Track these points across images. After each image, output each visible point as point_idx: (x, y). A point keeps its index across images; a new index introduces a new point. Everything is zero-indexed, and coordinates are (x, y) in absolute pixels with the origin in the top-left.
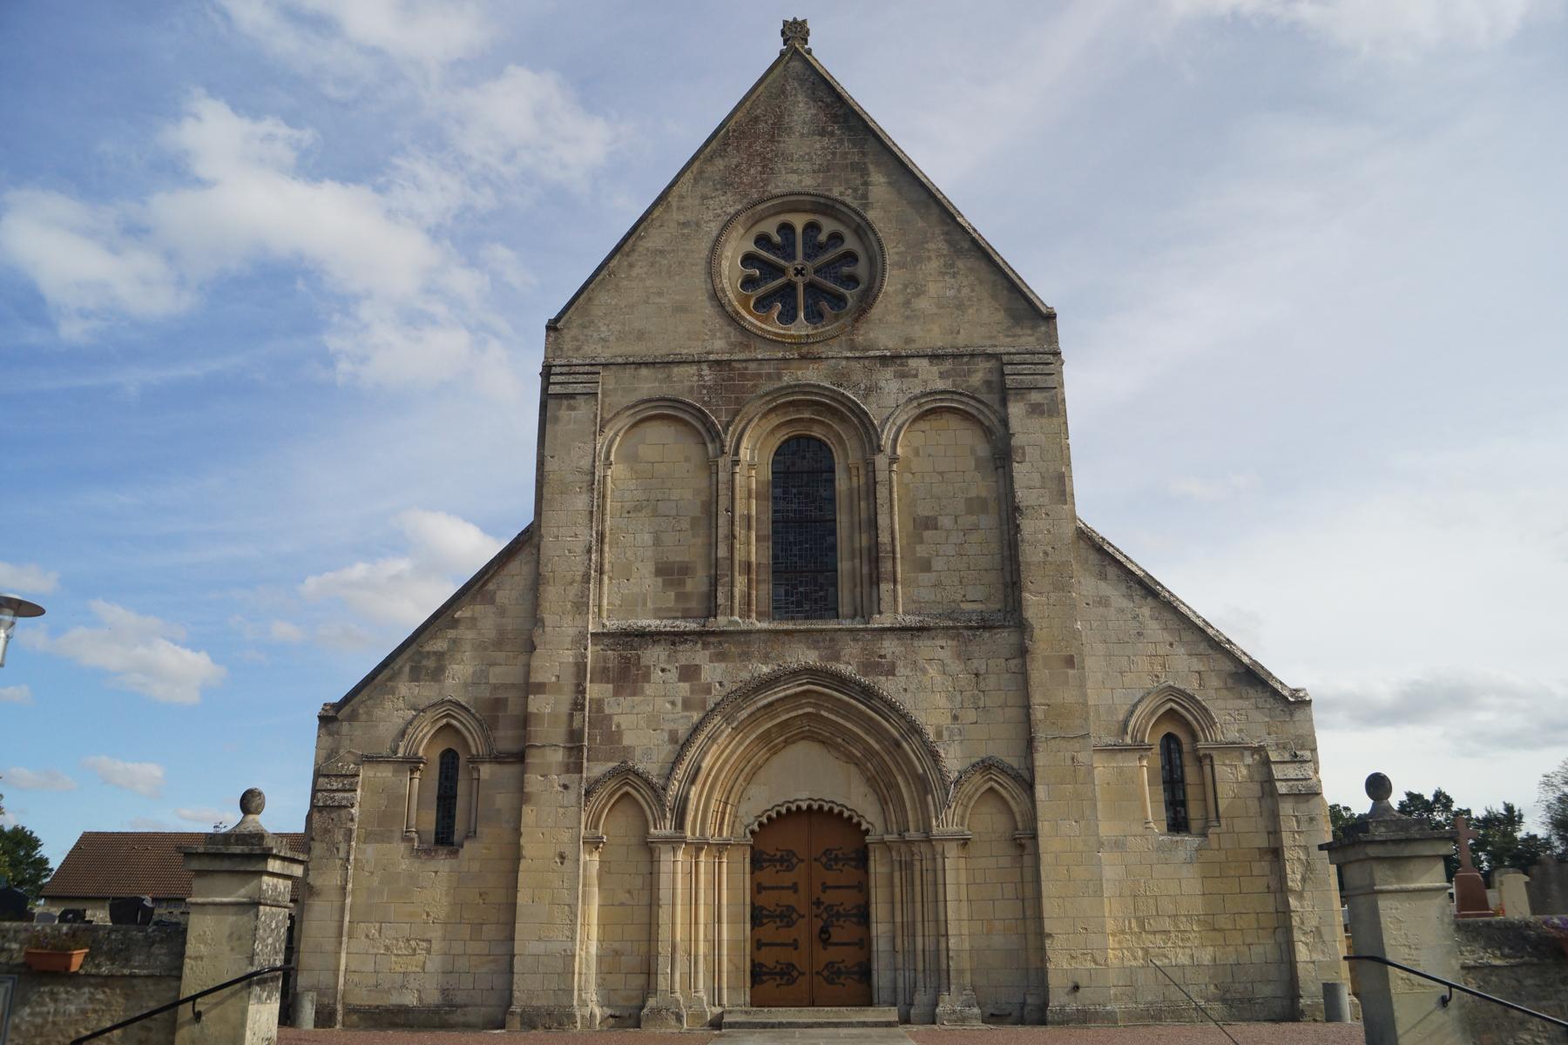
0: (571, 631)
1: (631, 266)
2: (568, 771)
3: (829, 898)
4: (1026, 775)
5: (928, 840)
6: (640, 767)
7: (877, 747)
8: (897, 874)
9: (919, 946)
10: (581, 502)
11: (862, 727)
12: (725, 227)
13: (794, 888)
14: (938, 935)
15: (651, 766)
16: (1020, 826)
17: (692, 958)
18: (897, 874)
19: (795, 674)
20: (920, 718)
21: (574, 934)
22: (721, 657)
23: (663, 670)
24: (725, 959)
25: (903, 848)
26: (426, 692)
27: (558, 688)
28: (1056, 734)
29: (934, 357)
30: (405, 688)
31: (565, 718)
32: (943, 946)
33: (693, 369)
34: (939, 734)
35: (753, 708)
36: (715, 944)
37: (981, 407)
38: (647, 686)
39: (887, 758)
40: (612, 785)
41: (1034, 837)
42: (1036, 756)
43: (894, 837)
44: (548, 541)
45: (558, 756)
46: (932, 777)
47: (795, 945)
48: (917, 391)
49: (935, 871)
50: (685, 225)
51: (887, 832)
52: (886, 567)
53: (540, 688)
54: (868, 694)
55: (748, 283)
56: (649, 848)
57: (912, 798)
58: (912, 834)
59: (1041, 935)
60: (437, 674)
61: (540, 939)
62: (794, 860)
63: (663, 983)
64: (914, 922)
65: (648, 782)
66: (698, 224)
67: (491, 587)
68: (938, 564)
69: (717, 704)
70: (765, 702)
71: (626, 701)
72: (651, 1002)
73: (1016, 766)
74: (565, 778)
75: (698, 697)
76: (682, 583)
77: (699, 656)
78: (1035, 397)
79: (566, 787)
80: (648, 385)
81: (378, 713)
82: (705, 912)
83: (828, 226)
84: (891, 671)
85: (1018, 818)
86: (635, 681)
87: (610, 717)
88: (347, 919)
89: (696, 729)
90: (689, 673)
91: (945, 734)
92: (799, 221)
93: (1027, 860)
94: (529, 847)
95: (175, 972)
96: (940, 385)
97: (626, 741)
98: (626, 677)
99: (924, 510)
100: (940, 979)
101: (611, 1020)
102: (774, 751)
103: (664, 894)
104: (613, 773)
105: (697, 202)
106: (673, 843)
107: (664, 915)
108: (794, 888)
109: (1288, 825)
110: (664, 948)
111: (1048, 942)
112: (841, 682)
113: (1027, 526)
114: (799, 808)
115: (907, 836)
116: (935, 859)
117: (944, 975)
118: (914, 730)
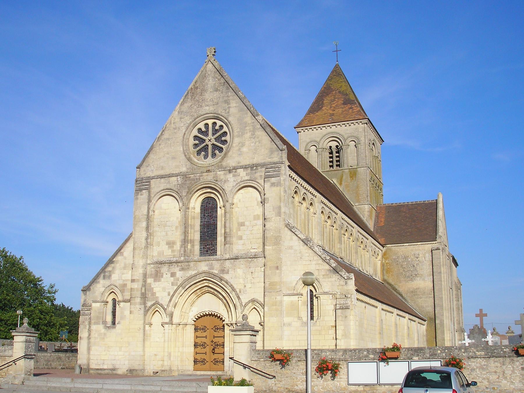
1: (160, 145)
3: (215, 340)
6: (161, 302)
10: (144, 224)
13: (206, 337)
26: (107, 282)
29: (245, 167)
31: (140, 289)
34: (240, 292)
37: (258, 184)
47: (206, 353)
54: (221, 279)
60: (110, 277)
66: (179, 128)
67: (122, 251)
68: (244, 237)
71: (157, 283)
76: (173, 247)
83: (219, 123)
84: (228, 273)
90: (173, 275)
92: (210, 122)
98: (157, 276)
99: (241, 220)
105: (179, 120)
108: (206, 337)
118: (234, 290)
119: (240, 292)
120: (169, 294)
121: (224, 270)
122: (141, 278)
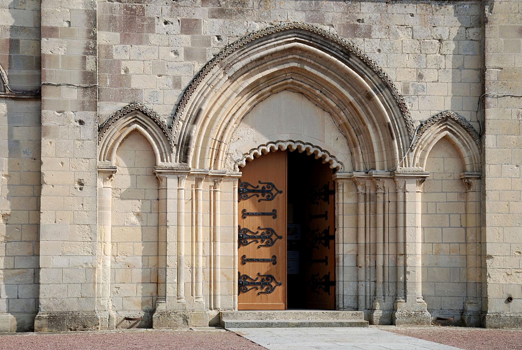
2: (83, 108)
4: (476, 126)
5: (393, 176)
6: (149, 107)
7: (351, 99)
8: (362, 205)
9: (380, 263)
11: (339, 82)
14: (397, 255)
15: (163, 111)
16: (468, 168)
17: (194, 270)
18: (362, 205)
19: (285, 31)
20: (392, 75)
23: (166, 23)
24: (219, 271)
25: (368, 184)
27: (69, 32)
28: (506, 93)
31: (78, 61)
32: (401, 263)
34: (406, 90)
35: (248, 60)
36: (212, 260)
38: (151, 36)
39: (359, 108)
40: (129, 119)
41: (481, 177)
42: (487, 110)
43: (362, 174)
45: (73, 95)
46: (399, 125)
49: (396, 203)
51: (354, 170)
54: (347, 53)
56: (157, 177)
57: (379, 144)
58: (378, 172)
59: (482, 256)
61: (63, 255)
62: (274, 192)
63: (171, 291)
64: (376, 244)
65: (155, 121)
69: (216, 56)
70: (258, 55)
71: (134, 49)
72: (162, 307)
73: (468, 119)
74: (81, 115)
79: (81, 122)
82: (211, 232)
84: (368, 34)
85: (467, 161)
86: (141, 31)
87: (119, 62)
91: (411, 90)
93: (472, 196)
97: (134, 85)
100: (399, 289)
101: (127, 323)
102: (261, 100)
103: (171, 217)
104: (125, 112)
106: (179, 174)
111: (488, 262)
112: (324, 41)
114: (280, 148)
115: (374, 174)
116: (396, 193)
117: (401, 286)
118: (386, 85)
119: (406, 90)
120: (177, 84)
121: (355, 28)
122: (81, 26)
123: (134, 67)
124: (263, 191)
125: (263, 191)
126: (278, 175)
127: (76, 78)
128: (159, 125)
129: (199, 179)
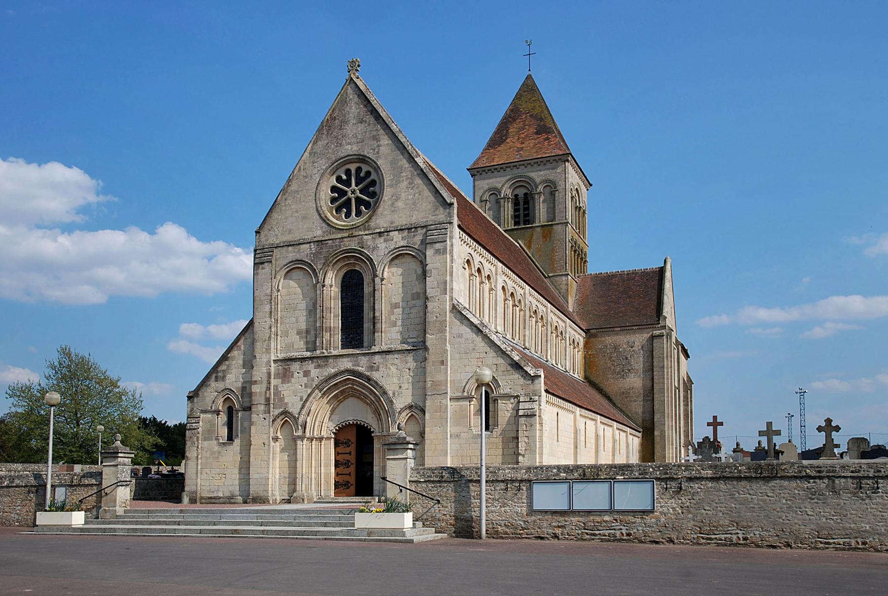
0: (265, 360)
6: (290, 410)
12: (322, 175)
15: (295, 411)
19: (342, 372)
21: (271, 473)
22: (319, 366)
26: (221, 385)
27: (261, 382)
30: (213, 384)
33: (307, 246)
34: (394, 394)
40: (283, 416)
44: (256, 324)
45: (262, 408)
48: (392, 247)
50: (306, 177)
52: (378, 326)
53: (255, 382)
54: (369, 379)
55: (333, 200)
60: (223, 378)
63: (298, 488)
71: (285, 386)
75: (310, 383)
77: (310, 366)
78: (438, 246)
80: (292, 254)
81: (206, 394)
82: (319, 464)
88: (199, 467)
89: (309, 396)
90: (306, 374)
92: (353, 167)
94: (254, 441)
95: (101, 484)
96: (402, 243)
98: (285, 376)
106: (302, 438)
107: (299, 464)
109: (522, 428)
110: (299, 476)
112: (360, 375)
113: (430, 305)
120: (301, 400)
123: (286, 393)
124: (346, 443)
125: (346, 443)
126: (352, 436)
127: (263, 402)
128: (294, 417)
129: (311, 439)
